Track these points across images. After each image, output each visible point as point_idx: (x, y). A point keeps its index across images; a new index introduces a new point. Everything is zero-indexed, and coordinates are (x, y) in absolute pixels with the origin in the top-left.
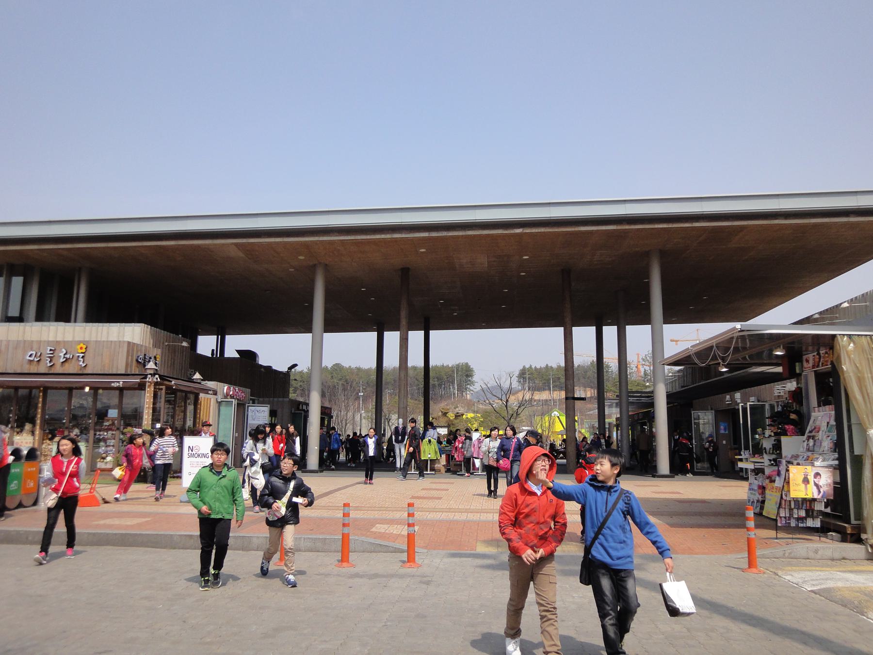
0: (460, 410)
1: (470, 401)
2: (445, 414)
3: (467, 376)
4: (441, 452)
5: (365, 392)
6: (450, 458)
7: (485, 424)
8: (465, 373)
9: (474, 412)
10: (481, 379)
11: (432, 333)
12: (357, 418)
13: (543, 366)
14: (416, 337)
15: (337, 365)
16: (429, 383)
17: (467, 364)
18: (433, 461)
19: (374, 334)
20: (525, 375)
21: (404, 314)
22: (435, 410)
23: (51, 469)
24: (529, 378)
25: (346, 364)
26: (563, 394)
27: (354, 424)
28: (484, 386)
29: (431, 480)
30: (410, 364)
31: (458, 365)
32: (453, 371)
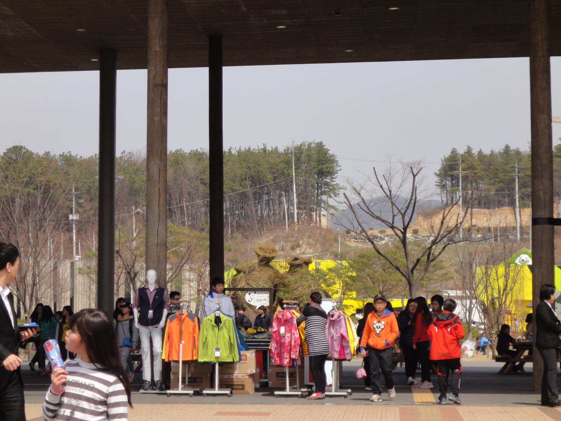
0: (304, 251)
1: (328, 230)
2: (266, 261)
3: (321, 173)
4: (245, 344)
5: (81, 212)
6: (263, 358)
7: (359, 284)
8: (317, 165)
9: (336, 256)
10: (356, 177)
11: (230, 73)
12: (65, 269)
13: (498, 148)
14: (188, 84)
15: (16, 150)
16: (223, 192)
17: (321, 143)
18: (227, 367)
19: (92, 78)
20: (457, 170)
21: (156, 27)
22: (241, 250)
23: (34, 347)
24: (465, 178)
25: (37, 147)
26: (525, 216)
27: (56, 285)
28: (355, 200)
29: (217, 408)
30: (172, 146)
31: (299, 150)
32: (288, 163)
